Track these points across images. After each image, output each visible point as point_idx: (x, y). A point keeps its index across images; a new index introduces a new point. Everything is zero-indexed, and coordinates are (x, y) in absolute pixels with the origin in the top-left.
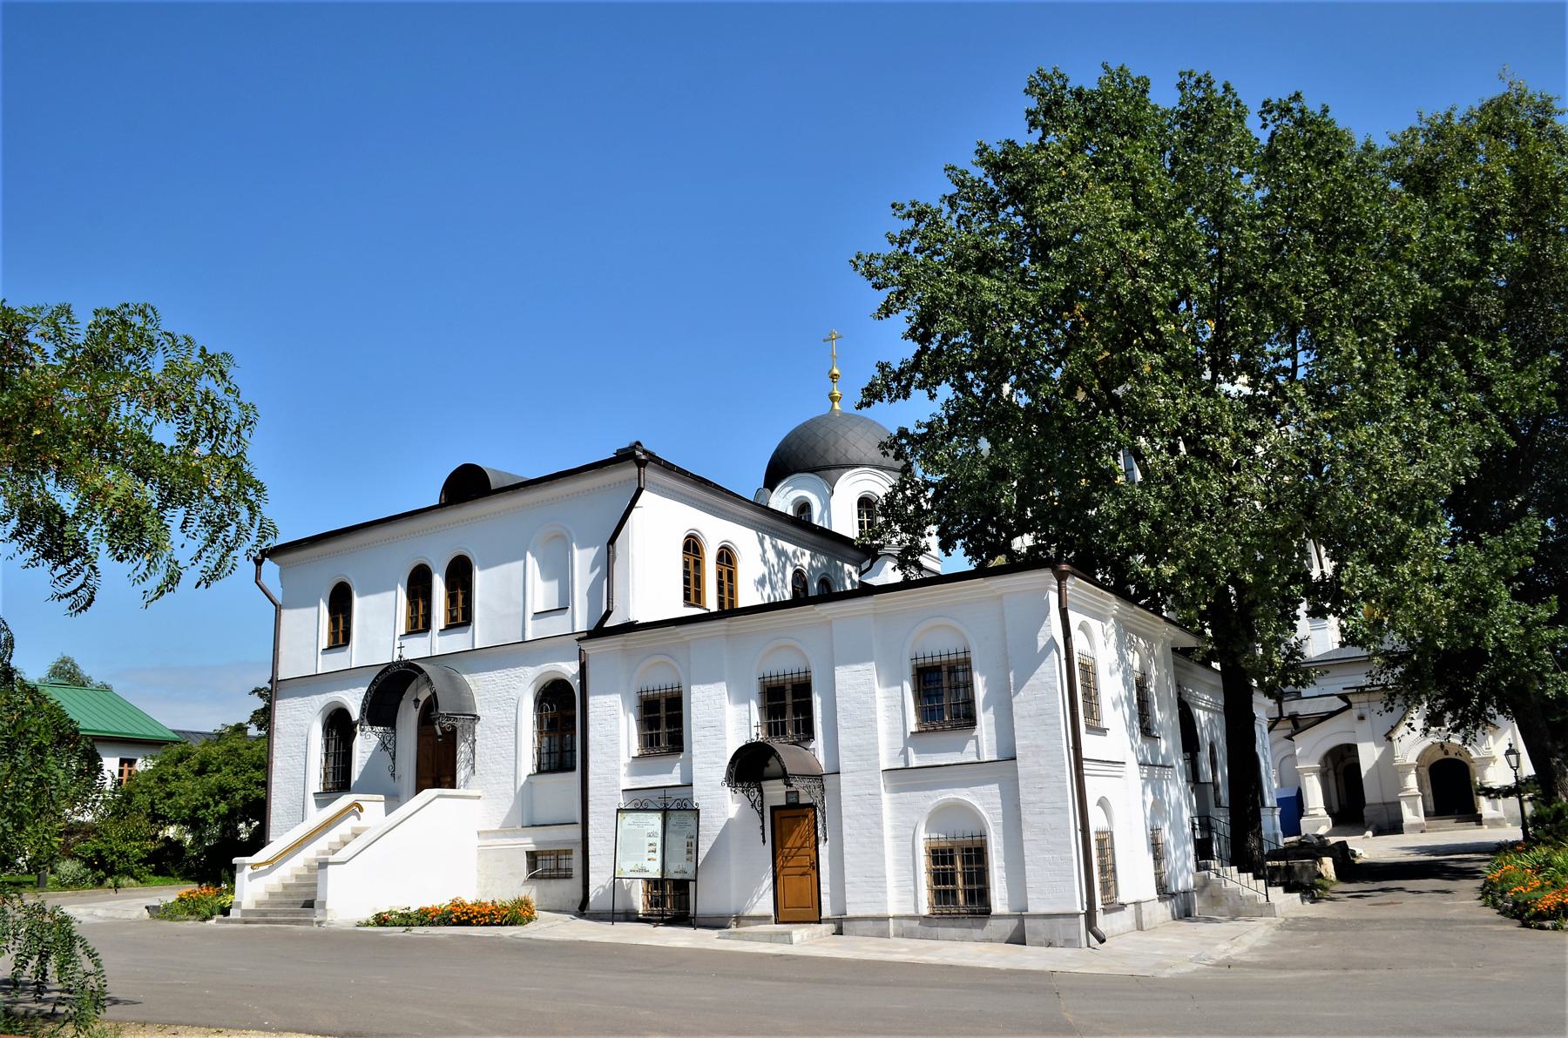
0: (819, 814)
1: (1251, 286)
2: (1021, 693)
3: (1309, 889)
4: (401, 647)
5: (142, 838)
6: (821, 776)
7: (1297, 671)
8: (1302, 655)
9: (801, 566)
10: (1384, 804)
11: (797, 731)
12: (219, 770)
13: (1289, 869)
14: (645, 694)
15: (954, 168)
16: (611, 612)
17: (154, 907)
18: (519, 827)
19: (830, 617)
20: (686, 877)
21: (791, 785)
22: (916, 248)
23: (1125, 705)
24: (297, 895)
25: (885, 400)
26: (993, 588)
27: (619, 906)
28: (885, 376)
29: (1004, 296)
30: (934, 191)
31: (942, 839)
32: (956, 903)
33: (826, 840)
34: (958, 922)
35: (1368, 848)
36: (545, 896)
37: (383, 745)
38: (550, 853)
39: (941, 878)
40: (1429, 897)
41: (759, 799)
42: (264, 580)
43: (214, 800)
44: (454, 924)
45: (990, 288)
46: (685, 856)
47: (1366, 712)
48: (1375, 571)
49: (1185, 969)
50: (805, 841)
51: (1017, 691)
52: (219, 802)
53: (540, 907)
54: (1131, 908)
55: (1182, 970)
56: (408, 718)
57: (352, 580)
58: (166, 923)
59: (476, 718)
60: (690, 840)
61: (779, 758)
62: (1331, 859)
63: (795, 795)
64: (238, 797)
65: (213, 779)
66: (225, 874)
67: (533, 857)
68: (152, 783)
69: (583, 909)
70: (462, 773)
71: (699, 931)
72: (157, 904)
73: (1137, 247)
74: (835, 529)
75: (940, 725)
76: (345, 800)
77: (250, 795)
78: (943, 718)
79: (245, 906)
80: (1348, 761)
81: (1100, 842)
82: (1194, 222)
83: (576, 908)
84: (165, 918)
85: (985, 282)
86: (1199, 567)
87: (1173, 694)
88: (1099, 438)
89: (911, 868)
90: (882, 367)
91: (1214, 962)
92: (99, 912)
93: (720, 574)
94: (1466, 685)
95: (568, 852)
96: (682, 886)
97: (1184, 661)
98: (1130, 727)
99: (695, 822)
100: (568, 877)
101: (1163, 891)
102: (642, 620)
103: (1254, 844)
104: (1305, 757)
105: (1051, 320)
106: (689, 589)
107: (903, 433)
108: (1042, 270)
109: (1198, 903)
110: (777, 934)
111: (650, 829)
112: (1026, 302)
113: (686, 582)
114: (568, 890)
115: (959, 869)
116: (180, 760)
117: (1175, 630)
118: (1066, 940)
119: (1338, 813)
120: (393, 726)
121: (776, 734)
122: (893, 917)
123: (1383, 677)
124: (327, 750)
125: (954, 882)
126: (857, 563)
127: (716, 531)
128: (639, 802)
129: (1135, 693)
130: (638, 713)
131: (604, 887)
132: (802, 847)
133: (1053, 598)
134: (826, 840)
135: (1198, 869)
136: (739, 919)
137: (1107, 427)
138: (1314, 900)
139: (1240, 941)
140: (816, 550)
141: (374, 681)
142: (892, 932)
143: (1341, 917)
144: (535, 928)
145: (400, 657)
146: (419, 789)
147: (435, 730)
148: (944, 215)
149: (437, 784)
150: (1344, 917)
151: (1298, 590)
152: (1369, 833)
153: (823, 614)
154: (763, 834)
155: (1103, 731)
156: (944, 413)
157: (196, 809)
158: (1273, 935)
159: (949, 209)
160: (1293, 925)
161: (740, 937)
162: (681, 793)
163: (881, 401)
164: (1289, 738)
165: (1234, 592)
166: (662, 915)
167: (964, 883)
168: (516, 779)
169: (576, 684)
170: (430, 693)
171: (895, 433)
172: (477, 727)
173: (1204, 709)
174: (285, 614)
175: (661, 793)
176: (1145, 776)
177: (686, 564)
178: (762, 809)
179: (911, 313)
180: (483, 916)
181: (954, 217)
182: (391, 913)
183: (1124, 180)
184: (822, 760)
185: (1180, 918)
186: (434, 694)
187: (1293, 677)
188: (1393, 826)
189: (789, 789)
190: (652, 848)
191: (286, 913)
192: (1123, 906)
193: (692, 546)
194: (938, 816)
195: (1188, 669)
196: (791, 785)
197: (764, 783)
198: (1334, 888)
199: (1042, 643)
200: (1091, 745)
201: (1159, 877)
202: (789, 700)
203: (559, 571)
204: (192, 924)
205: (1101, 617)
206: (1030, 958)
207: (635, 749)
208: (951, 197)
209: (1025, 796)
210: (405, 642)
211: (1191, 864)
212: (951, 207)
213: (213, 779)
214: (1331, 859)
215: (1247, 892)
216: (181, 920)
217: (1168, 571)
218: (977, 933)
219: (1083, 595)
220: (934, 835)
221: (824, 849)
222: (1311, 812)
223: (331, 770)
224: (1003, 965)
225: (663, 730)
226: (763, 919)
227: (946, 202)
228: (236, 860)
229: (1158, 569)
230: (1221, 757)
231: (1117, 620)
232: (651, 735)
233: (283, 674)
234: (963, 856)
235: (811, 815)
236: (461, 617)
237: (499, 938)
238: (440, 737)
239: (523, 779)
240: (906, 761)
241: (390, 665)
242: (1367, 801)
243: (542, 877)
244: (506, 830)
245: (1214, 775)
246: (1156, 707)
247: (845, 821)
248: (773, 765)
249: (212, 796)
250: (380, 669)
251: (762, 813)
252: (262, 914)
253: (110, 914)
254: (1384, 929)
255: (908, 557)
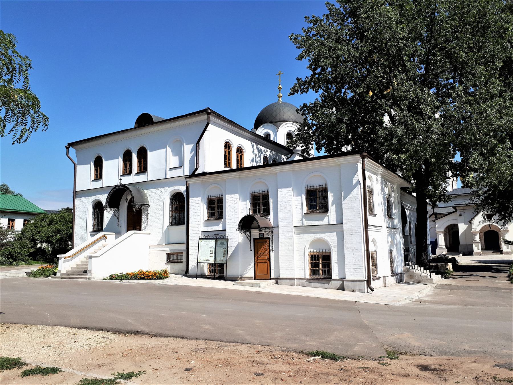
0: (271, 241)
1: (442, 49)
2: (346, 200)
3: (444, 274)
4: (120, 180)
5: (27, 248)
6: (272, 228)
7: (445, 197)
8: (447, 191)
9: (266, 155)
10: (467, 245)
11: (264, 212)
12: (57, 224)
13: (437, 266)
14: (210, 198)
15: (329, 3)
16: (198, 168)
17: (28, 272)
18: (164, 244)
19: (276, 172)
20: (223, 262)
21: (261, 231)
22: (313, 35)
23: (383, 206)
24: (82, 268)
25: (299, 93)
26: (337, 161)
27: (199, 272)
28: (299, 83)
29: (346, 52)
30: (321, 12)
31: (314, 251)
32: (319, 274)
33: (273, 250)
34: (320, 281)
35: (463, 260)
36: (173, 269)
37: (115, 215)
38: (175, 254)
39: (314, 265)
40: (489, 279)
41: (250, 235)
42: (70, 155)
43: (55, 234)
44: (139, 279)
45: (341, 50)
46: (223, 255)
47: (462, 213)
48: (482, 159)
49: (405, 302)
50: (266, 251)
51: (344, 199)
52: (57, 235)
53: (171, 273)
54: (382, 278)
55: (404, 303)
56: (124, 206)
57: (103, 155)
58: (32, 278)
59: (148, 206)
60: (225, 250)
61: (257, 221)
62: (451, 263)
63: (262, 234)
64: (64, 233)
65: (54, 227)
66: (55, 260)
67: (169, 255)
68: (32, 228)
69: (186, 274)
70: (143, 225)
71: (227, 282)
72: (30, 271)
73: (401, 30)
74: (278, 142)
75: (315, 211)
76: (101, 234)
77: (68, 232)
78: (316, 208)
79: (62, 272)
80: (454, 230)
81: (372, 255)
82: (421, 24)
83: (184, 273)
84: (32, 277)
85: (340, 46)
86: (414, 156)
87: (399, 203)
88: (377, 108)
89: (303, 262)
90: (299, 80)
91: (414, 300)
92: (8, 274)
93: (237, 157)
94: (507, 203)
95: (182, 253)
96: (222, 266)
97: (403, 192)
98: (384, 215)
99: (227, 243)
100: (182, 262)
101: (393, 273)
102: (209, 172)
103: (425, 257)
104: (439, 228)
105: (362, 65)
106: (226, 161)
107: (305, 105)
108: (361, 43)
109: (405, 277)
110: (255, 284)
111: (211, 245)
112: (354, 55)
113: (225, 159)
114: (181, 267)
115: (321, 262)
116: (43, 220)
117: (402, 180)
118: (359, 290)
119: (449, 247)
120: (118, 209)
121: (256, 213)
122: (296, 279)
123: (475, 200)
124: (94, 216)
125: (318, 267)
126: (286, 155)
127: (236, 141)
128: (207, 236)
129: (386, 202)
130: (207, 204)
131: (194, 266)
132: (264, 253)
133: (360, 166)
134: (273, 250)
135: (405, 266)
136: (242, 278)
137: (382, 104)
138: (446, 278)
139: (422, 292)
140: (272, 150)
141: (111, 192)
142: (296, 284)
143: (458, 285)
144: (168, 280)
145: (120, 183)
146: (128, 230)
147: (133, 209)
148: (325, 22)
149: (134, 229)
150: (459, 285)
151: (447, 167)
152: (461, 255)
153: (274, 170)
154: (251, 248)
155: (375, 215)
156: (320, 98)
157: (48, 237)
158: (434, 290)
159: (326, 20)
160: (440, 287)
161: (242, 285)
162: (222, 233)
163: (298, 93)
164: (434, 221)
165: (424, 167)
166: (214, 276)
167: (322, 267)
168: (163, 228)
169: (185, 194)
170: (131, 197)
171: (302, 105)
172: (149, 208)
173: (408, 209)
174: (78, 167)
175: (215, 233)
176: (389, 232)
177: (225, 152)
178: (251, 239)
179: (310, 59)
180: (149, 276)
181: (328, 23)
182: (115, 275)
183: (397, 5)
184: (272, 223)
185: (399, 283)
186: (133, 197)
187: (443, 198)
188: (470, 253)
189: (260, 232)
190: (211, 252)
191: (78, 275)
192: (379, 278)
193: (227, 146)
194: (313, 243)
195: (403, 195)
196: (261, 231)
197: (251, 230)
198: (452, 274)
199: (354, 182)
200: (371, 220)
201: (392, 267)
202: (261, 201)
203: (179, 152)
204: (42, 279)
205: (376, 174)
206: (346, 296)
207: (206, 217)
208: (327, 15)
209: (346, 237)
210: (121, 178)
211: (403, 264)
212: (327, 19)
213: (54, 227)
214: (451, 263)
215: (423, 274)
216: (38, 277)
217: (403, 157)
218: (326, 285)
219: (370, 165)
220: (312, 250)
221: (272, 254)
222: (440, 247)
223: (96, 224)
224: (337, 298)
225: (216, 211)
226: (250, 278)
227: (325, 17)
228: (58, 256)
229: (399, 156)
230: (413, 227)
231: (382, 175)
232: (212, 213)
233: (77, 190)
234: (322, 258)
235: (268, 241)
236: (143, 169)
237: (154, 284)
238: (135, 212)
239: (165, 227)
240: (303, 223)
241: (116, 186)
242: (460, 244)
243: (172, 262)
244: (159, 245)
245: (410, 233)
246: (393, 208)
247: (280, 244)
248: (255, 224)
249: (55, 233)
250: (114, 187)
251: (250, 241)
252: (68, 275)
253: (12, 275)
254: (475, 290)
255: (306, 150)
